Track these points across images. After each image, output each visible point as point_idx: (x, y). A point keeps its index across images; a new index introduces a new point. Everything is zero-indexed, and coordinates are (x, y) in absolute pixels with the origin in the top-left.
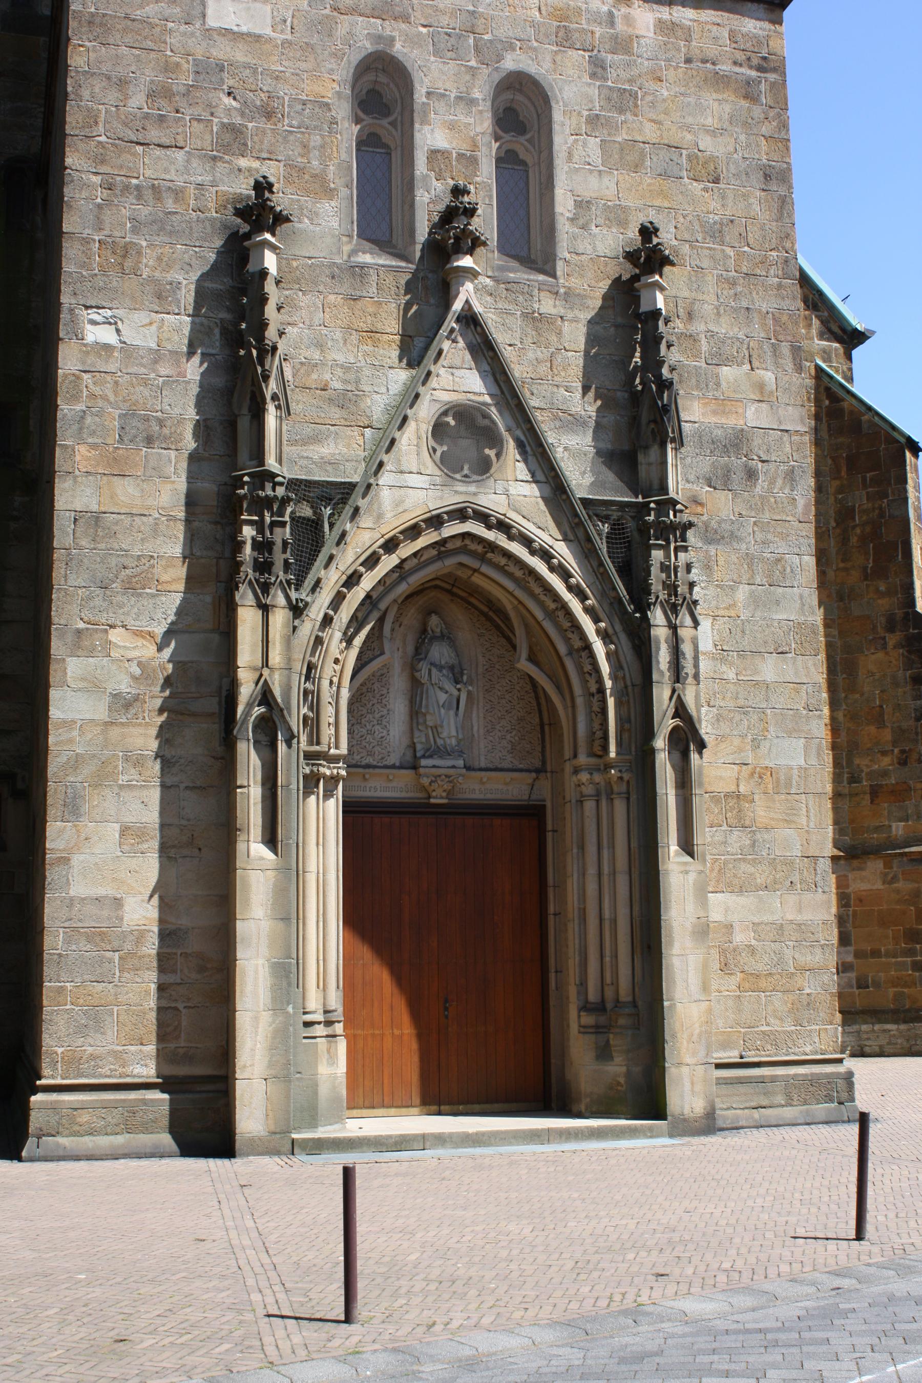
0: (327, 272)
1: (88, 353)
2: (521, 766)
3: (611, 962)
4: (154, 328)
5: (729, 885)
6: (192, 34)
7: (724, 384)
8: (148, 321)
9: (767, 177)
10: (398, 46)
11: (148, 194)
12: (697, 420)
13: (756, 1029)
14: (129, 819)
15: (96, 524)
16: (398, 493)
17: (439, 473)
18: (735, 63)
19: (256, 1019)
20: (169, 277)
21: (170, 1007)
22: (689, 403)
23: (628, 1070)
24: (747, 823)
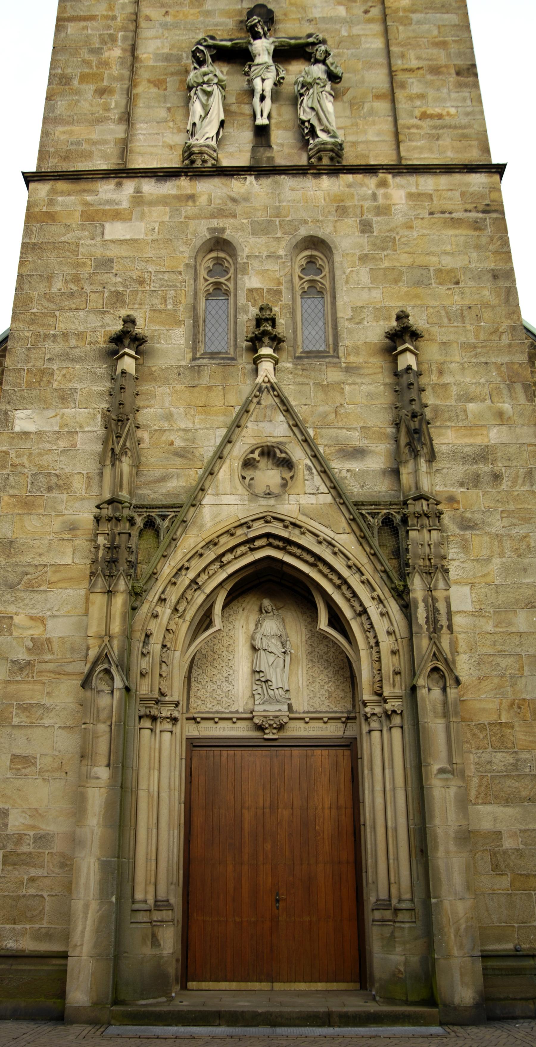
0: (176, 371)
1: (13, 438)
2: (335, 709)
3: (394, 863)
4: (58, 417)
5: (496, 797)
6: (95, 245)
7: (470, 416)
8: (54, 414)
9: (495, 277)
10: (228, 231)
11: (60, 339)
12: (450, 442)
13: (529, 924)
14: (17, 752)
15: (10, 546)
16: (215, 509)
17: (247, 493)
18: (466, 211)
19: (87, 906)
20: (70, 385)
21: (37, 895)
22: (444, 431)
23: (406, 959)
24: (510, 745)
